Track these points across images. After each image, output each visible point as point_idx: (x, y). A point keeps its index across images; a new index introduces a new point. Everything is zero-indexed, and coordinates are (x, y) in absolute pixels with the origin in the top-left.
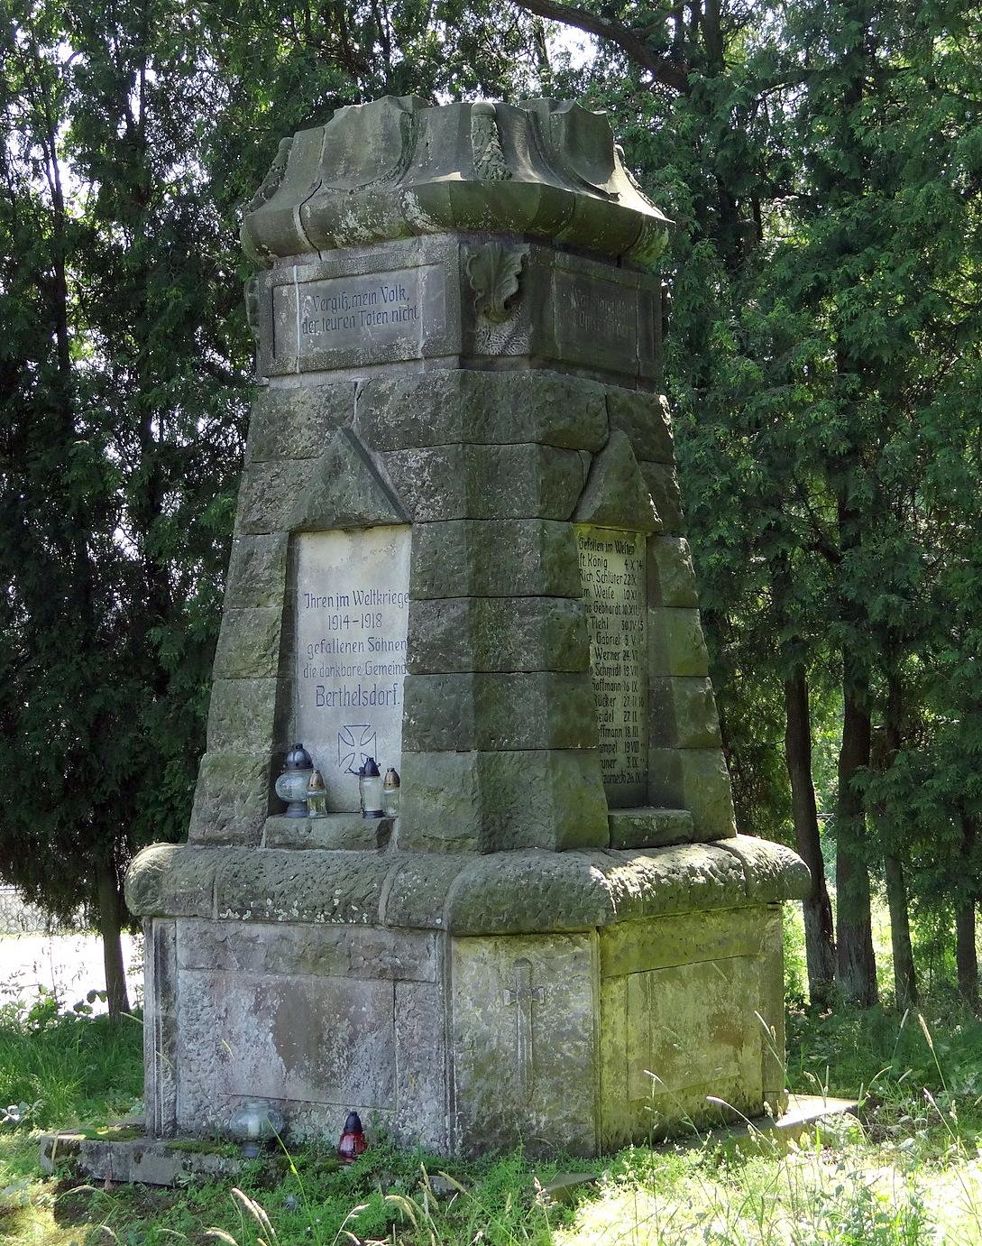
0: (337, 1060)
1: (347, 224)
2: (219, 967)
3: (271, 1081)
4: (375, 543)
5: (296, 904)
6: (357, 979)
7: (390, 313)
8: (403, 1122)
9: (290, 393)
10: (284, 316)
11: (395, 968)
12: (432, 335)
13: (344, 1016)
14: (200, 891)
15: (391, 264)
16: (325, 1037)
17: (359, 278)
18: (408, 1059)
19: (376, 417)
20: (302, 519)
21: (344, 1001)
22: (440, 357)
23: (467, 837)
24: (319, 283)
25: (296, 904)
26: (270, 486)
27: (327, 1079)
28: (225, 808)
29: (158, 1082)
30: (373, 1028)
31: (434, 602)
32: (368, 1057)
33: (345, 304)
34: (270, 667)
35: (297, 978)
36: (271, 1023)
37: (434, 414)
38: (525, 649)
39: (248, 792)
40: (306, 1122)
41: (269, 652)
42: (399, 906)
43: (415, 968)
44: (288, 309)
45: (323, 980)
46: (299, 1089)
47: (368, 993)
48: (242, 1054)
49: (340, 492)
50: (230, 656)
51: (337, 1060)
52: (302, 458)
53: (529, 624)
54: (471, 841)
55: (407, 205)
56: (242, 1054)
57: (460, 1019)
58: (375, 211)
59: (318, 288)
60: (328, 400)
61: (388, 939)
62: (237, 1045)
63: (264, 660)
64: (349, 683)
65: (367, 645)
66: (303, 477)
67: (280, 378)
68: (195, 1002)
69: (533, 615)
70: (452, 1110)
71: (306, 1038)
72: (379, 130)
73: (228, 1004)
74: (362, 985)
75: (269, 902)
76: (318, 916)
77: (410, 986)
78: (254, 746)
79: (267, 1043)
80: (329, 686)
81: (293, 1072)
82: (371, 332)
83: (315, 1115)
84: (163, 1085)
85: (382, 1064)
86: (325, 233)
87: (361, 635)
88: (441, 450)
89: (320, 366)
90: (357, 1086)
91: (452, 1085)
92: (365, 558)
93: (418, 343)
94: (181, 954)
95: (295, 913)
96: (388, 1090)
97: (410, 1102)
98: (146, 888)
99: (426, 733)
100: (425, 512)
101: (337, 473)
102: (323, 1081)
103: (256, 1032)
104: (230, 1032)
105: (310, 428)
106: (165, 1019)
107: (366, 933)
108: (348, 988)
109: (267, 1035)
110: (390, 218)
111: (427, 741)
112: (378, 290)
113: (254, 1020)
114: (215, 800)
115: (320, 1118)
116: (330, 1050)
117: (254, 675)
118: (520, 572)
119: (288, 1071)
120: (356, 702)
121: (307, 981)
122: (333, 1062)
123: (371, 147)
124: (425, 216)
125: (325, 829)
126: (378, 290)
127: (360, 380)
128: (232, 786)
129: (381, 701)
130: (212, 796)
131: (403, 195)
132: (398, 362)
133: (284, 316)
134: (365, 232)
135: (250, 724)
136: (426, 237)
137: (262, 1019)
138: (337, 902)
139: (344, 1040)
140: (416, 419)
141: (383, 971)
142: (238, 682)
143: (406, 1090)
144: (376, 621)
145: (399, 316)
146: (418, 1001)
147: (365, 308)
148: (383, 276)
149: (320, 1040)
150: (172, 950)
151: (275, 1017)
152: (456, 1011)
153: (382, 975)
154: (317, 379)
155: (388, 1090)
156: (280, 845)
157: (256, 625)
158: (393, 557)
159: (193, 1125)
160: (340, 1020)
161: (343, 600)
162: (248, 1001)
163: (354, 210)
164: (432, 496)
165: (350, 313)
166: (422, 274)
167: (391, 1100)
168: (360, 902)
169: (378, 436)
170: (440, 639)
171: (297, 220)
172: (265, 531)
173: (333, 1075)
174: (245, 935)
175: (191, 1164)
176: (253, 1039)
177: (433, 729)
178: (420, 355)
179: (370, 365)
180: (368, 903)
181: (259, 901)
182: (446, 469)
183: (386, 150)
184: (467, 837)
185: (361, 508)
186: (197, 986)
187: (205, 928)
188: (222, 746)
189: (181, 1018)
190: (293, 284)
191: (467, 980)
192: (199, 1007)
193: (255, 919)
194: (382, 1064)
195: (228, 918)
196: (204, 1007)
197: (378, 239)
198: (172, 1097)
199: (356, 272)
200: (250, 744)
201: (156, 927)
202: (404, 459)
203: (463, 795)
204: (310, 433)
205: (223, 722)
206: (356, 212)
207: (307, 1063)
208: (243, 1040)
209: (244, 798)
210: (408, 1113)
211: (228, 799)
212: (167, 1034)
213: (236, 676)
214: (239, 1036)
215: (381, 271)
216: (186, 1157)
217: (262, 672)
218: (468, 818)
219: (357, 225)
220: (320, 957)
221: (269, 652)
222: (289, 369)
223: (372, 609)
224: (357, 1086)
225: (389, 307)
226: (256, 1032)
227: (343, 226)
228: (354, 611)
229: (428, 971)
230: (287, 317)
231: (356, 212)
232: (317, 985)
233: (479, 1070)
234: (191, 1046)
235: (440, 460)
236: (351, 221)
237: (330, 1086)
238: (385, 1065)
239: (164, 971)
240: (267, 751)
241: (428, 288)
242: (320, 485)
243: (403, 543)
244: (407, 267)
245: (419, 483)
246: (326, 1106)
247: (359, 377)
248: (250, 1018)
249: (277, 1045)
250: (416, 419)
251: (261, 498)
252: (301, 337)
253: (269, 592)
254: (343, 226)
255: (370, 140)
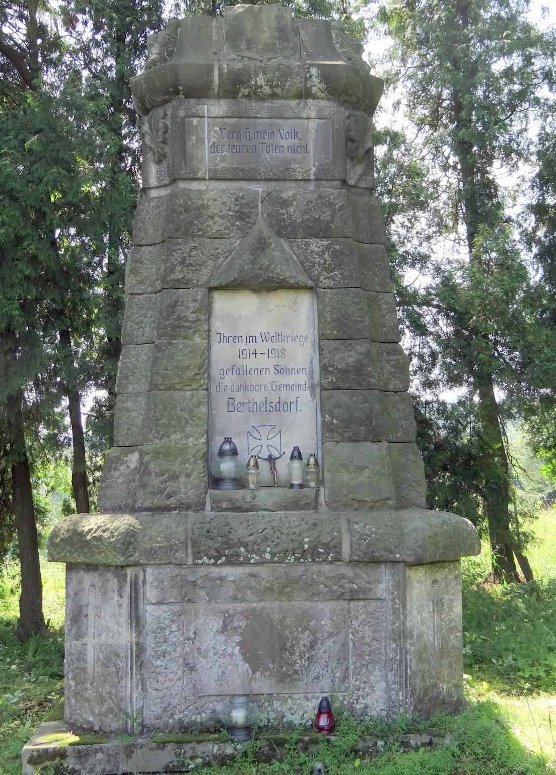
0: (299, 661)
1: (256, 82)
2: (189, 601)
3: (238, 682)
4: (280, 301)
5: (268, 549)
6: (317, 601)
7: (285, 147)
8: (358, 700)
9: (200, 192)
10: (194, 138)
11: (352, 591)
12: (321, 165)
13: (305, 629)
14: (176, 544)
15: (288, 114)
16: (288, 645)
17: (260, 120)
18: (360, 656)
19: (283, 214)
20: (232, 279)
21: (303, 620)
22: (327, 180)
23: (387, 499)
24: (226, 120)
25: (268, 549)
26: (190, 256)
27: (290, 676)
28: (172, 484)
29: (131, 693)
30: (330, 635)
31: (341, 342)
32: (326, 656)
33: (248, 137)
34: (202, 382)
35: (262, 604)
36: (237, 639)
37: (333, 216)
38: (393, 376)
39: (192, 471)
40: (269, 709)
41: (202, 372)
42: (363, 547)
43: (370, 590)
44: (197, 134)
45: (286, 604)
46: (263, 685)
47: (327, 611)
48: (210, 664)
49: (269, 262)
50: (166, 374)
51: (299, 661)
52: (216, 238)
53: (393, 360)
54: (390, 502)
55: (311, 76)
56: (210, 664)
57: (412, 623)
58: (281, 76)
59: (225, 123)
60: (236, 200)
61: (348, 572)
62: (205, 658)
63: (198, 377)
64: (258, 397)
65: (272, 370)
66: (219, 251)
67: (188, 182)
68: (163, 629)
69: (395, 355)
70: (406, 687)
71: (270, 648)
72: (274, 24)
73: (196, 628)
74: (321, 605)
75: (242, 549)
76: (289, 558)
77: (361, 603)
78: (191, 439)
79: (233, 654)
80: (239, 397)
81: (258, 673)
82: (269, 159)
83: (276, 704)
84: (135, 695)
85: (339, 660)
86: (234, 87)
87: (268, 363)
88: (337, 241)
89: (227, 176)
90: (317, 679)
91: (406, 669)
92: (271, 310)
93: (310, 169)
94: (151, 593)
95: (268, 556)
96: (345, 678)
97: (362, 685)
98: (130, 543)
99: (347, 430)
100: (327, 281)
101: (263, 249)
102: (287, 677)
103: (224, 647)
104: (199, 649)
105: (222, 217)
106: (137, 644)
107: (326, 568)
108: (309, 608)
109: (234, 648)
110: (296, 83)
111: (347, 435)
112: (275, 130)
113: (221, 638)
114: (161, 478)
115: (281, 705)
116: (292, 654)
117: (187, 388)
118: (385, 326)
119: (254, 673)
120: (263, 409)
121: (272, 606)
122: (295, 663)
123: (266, 35)
124: (322, 86)
125: (265, 497)
126: (275, 130)
127: (260, 190)
128: (176, 467)
129: (285, 409)
130: (157, 475)
131: (308, 68)
132: (291, 180)
133: (194, 138)
134: (267, 90)
135: (187, 422)
136: (311, 101)
137: (229, 637)
138: (306, 546)
139: (305, 646)
140: (319, 219)
141: (342, 594)
142: (172, 392)
143: (358, 677)
144: (280, 354)
145: (294, 149)
146: (367, 613)
147: (265, 141)
148: (281, 122)
149: (284, 648)
150: (142, 591)
151: (241, 634)
152: (409, 618)
153: (340, 597)
154: (224, 185)
155: (345, 678)
156: (226, 509)
157: (189, 352)
158: (295, 311)
159: (160, 723)
160: (302, 632)
161: (252, 338)
162: (216, 624)
163: (264, 73)
164: (332, 271)
165: (252, 143)
166: (313, 124)
167: (347, 685)
168: (326, 546)
169: (285, 228)
170: (353, 366)
171: (216, 73)
172: (186, 287)
173: (296, 672)
174: (214, 575)
175: (185, 752)
176: (221, 652)
177: (353, 427)
178: (312, 177)
179: (270, 180)
180: (337, 548)
181: (235, 549)
182: (343, 254)
183: (279, 38)
184: (387, 499)
185: (287, 274)
186: (166, 616)
187: (176, 572)
188: (161, 439)
189: (149, 642)
190: (208, 117)
191: (414, 596)
192: (167, 632)
193: (229, 563)
194: (339, 660)
195: (203, 564)
196: (171, 632)
197: (274, 96)
198: (141, 704)
199: (259, 116)
200: (187, 437)
201: (131, 574)
202: (307, 244)
203: (383, 471)
204: (222, 221)
205: (161, 421)
206: (266, 74)
207: (271, 666)
208: (211, 654)
209: (188, 476)
210: (360, 693)
211: (175, 477)
212: (138, 656)
213: (171, 388)
214: (207, 651)
215: (280, 118)
216: (180, 748)
217: (194, 386)
218: (386, 488)
219: (264, 83)
220: (286, 588)
221: (202, 372)
222: (199, 176)
223: (277, 346)
224: (317, 679)
225: (284, 143)
226: (224, 647)
227: (253, 83)
228: (260, 346)
229: (380, 592)
230: (197, 140)
231: (266, 74)
232: (281, 607)
233: (420, 659)
234: (158, 663)
235: (337, 247)
236: (261, 80)
237: (293, 680)
238: (342, 661)
239: (137, 608)
240: (203, 443)
241: (317, 134)
242: (247, 256)
243: (305, 303)
244: (302, 118)
245: (322, 262)
246: (287, 696)
247: (259, 188)
248: (218, 637)
249: (243, 654)
250: (319, 219)
251: (182, 263)
252: (209, 155)
253: (196, 329)
254: (253, 83)
255: (266, 29)
